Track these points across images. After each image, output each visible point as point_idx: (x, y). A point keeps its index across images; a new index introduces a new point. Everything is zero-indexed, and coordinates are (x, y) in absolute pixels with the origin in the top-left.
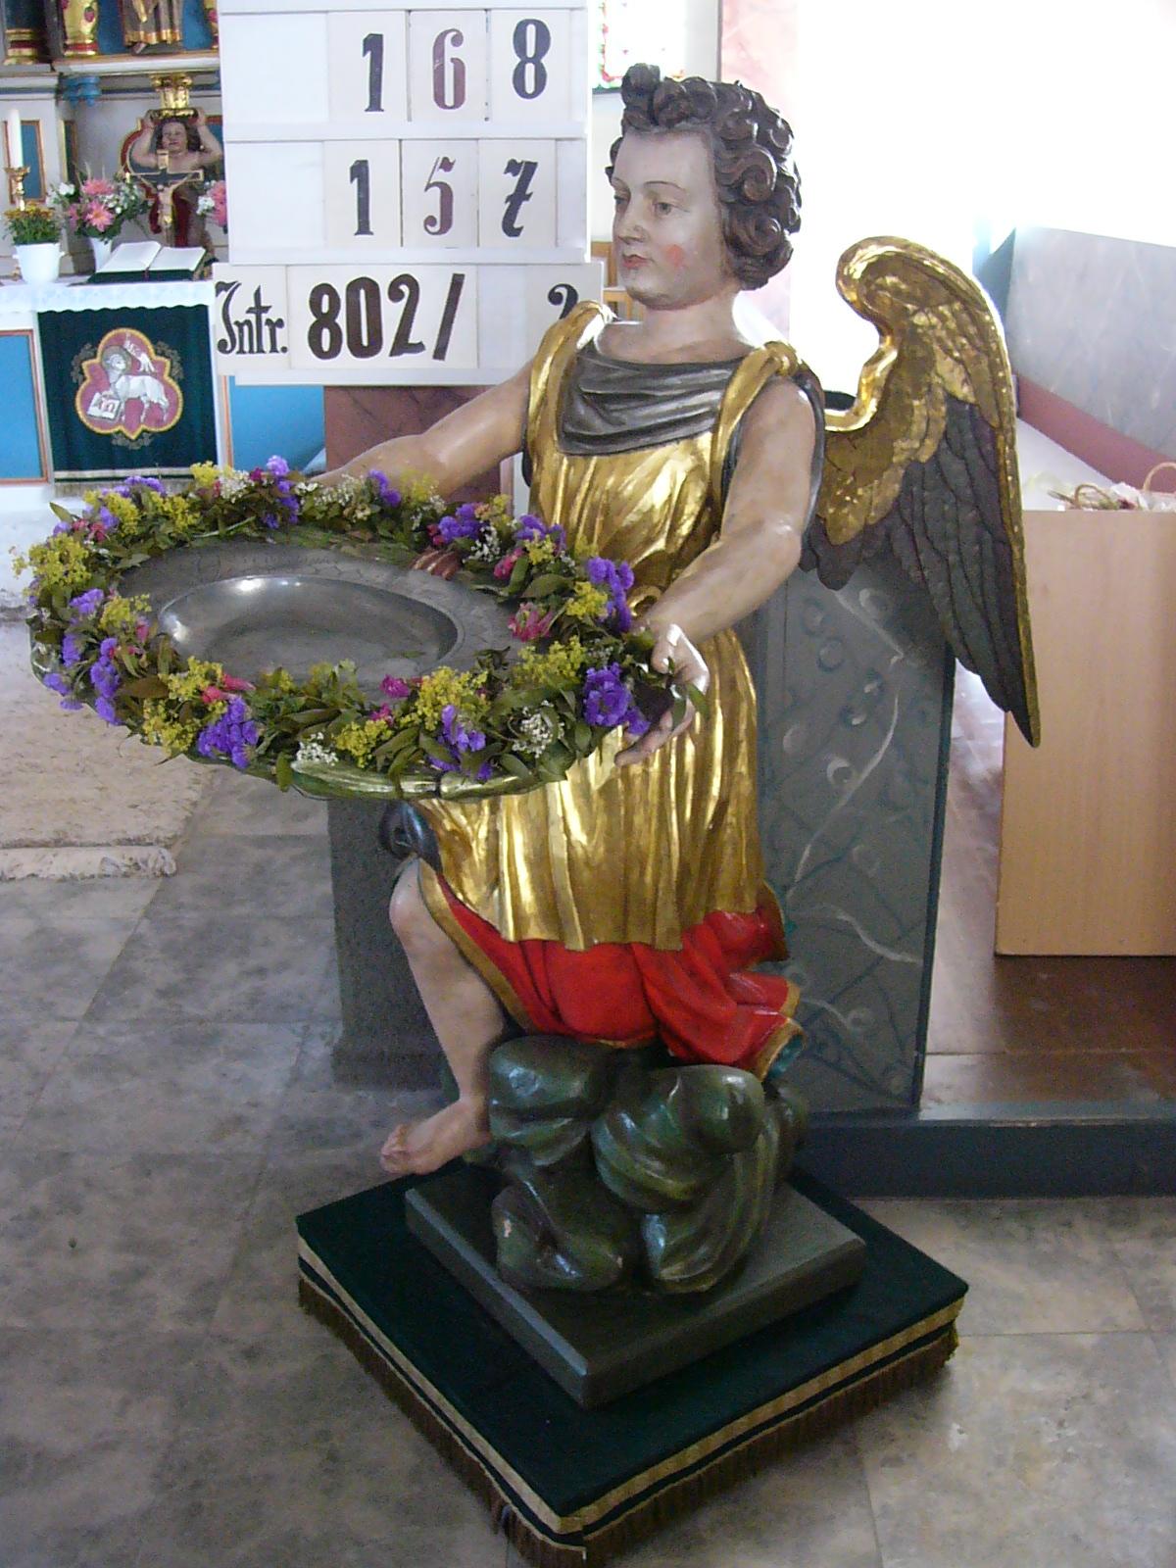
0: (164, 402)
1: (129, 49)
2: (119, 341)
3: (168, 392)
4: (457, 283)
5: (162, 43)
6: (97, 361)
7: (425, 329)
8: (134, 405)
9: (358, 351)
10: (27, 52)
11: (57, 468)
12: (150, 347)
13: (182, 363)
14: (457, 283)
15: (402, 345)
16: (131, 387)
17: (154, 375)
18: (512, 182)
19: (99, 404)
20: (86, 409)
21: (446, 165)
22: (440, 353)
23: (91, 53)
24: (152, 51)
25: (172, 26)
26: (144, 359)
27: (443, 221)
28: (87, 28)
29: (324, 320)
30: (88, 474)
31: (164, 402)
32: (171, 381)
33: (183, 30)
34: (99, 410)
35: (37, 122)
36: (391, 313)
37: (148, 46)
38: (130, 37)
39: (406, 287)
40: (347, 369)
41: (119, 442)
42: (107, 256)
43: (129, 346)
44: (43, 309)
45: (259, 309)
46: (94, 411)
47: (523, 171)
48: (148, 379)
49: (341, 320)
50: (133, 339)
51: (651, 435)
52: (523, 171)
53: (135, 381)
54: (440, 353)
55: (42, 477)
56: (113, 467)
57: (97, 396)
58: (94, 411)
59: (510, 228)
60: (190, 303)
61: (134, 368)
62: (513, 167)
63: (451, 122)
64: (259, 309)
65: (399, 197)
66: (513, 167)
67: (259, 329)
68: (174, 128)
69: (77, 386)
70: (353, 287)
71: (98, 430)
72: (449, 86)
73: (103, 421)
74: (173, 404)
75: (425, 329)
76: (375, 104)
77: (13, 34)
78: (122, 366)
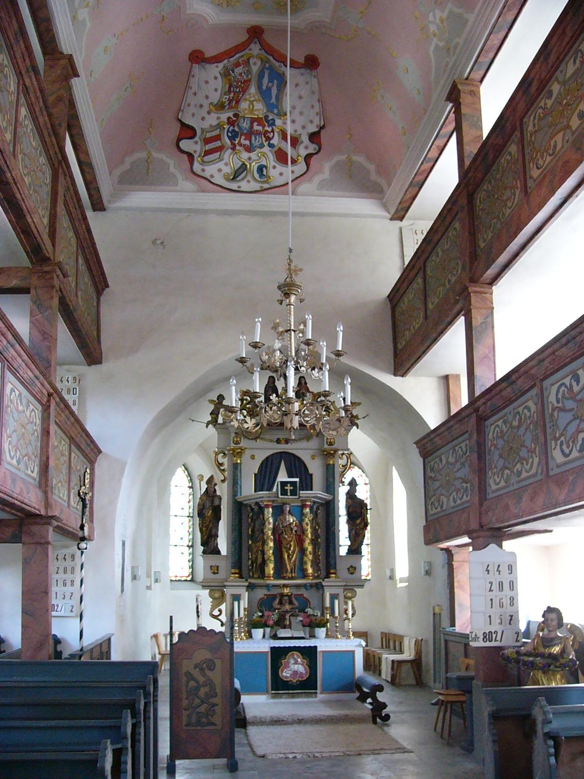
0: (304, 672)
1: (284, 578)
2: (293, 655)
3: (305, 669)
4: (503, 632)
5: (292, 576)
6: (286, 660)
7: (499, 638)
8: (295, 672)
9: (490, 641)
10: (237, 575)
11: (272, 690)
12: (301, 657)
13: (310, 661)
14: (503, 632)
15: (496, 640)
16: (295, 667)
17: (302, 664)
18: (510, 618)
19: (286, 672)
20: (282, 674)
21: (501, 615)
22: (501, 641)
23: (272, 578)
24: (289, 579)
25: (295, 573)
26: (299, 660)
27: (501, 623)
28: (272, 572)
29: (485, 637)
30: (281, 692)
31: (304, 672)
32: (306, 666)
33: (297, 574)
34: (285, 674)
35: (240, 595)
36: (494, 636)
37: (289, 577)
38: (285, 575)
39: (496, 632)
40: (488, 644)
41: (290, 683)
42: (282, 633)
43: (295, 656)
44: (272, 646)
45: (476, 635)
46: (284, 674)
47: (512, 616)
48: (300, 666)
49: (487, 637)
50: (297, 655)
51: (555, 645)
52: (512, 616)
53: (296, 666)
54: (501, 641)
55: (267, 692)
56: (288, 690)
57: (285, 670)
58: (284, 674)
59: (510, 624)
60: (312, 645)
61: (296, 663)
62: (510, 616)
63: (503, 610)
64: (476, 635)
65: (496, 620)
66: (510, 616)
67: (476, 639)
68: (286, 598)
69: (280, 667)
70: (489, 632)
71: (285, 679)
72: (501, 605)
73: (286, 677)
74: (306, 673)
75: (499, 638)
76: (492, 607)
77: (233, 571)
78: (293, 662)
